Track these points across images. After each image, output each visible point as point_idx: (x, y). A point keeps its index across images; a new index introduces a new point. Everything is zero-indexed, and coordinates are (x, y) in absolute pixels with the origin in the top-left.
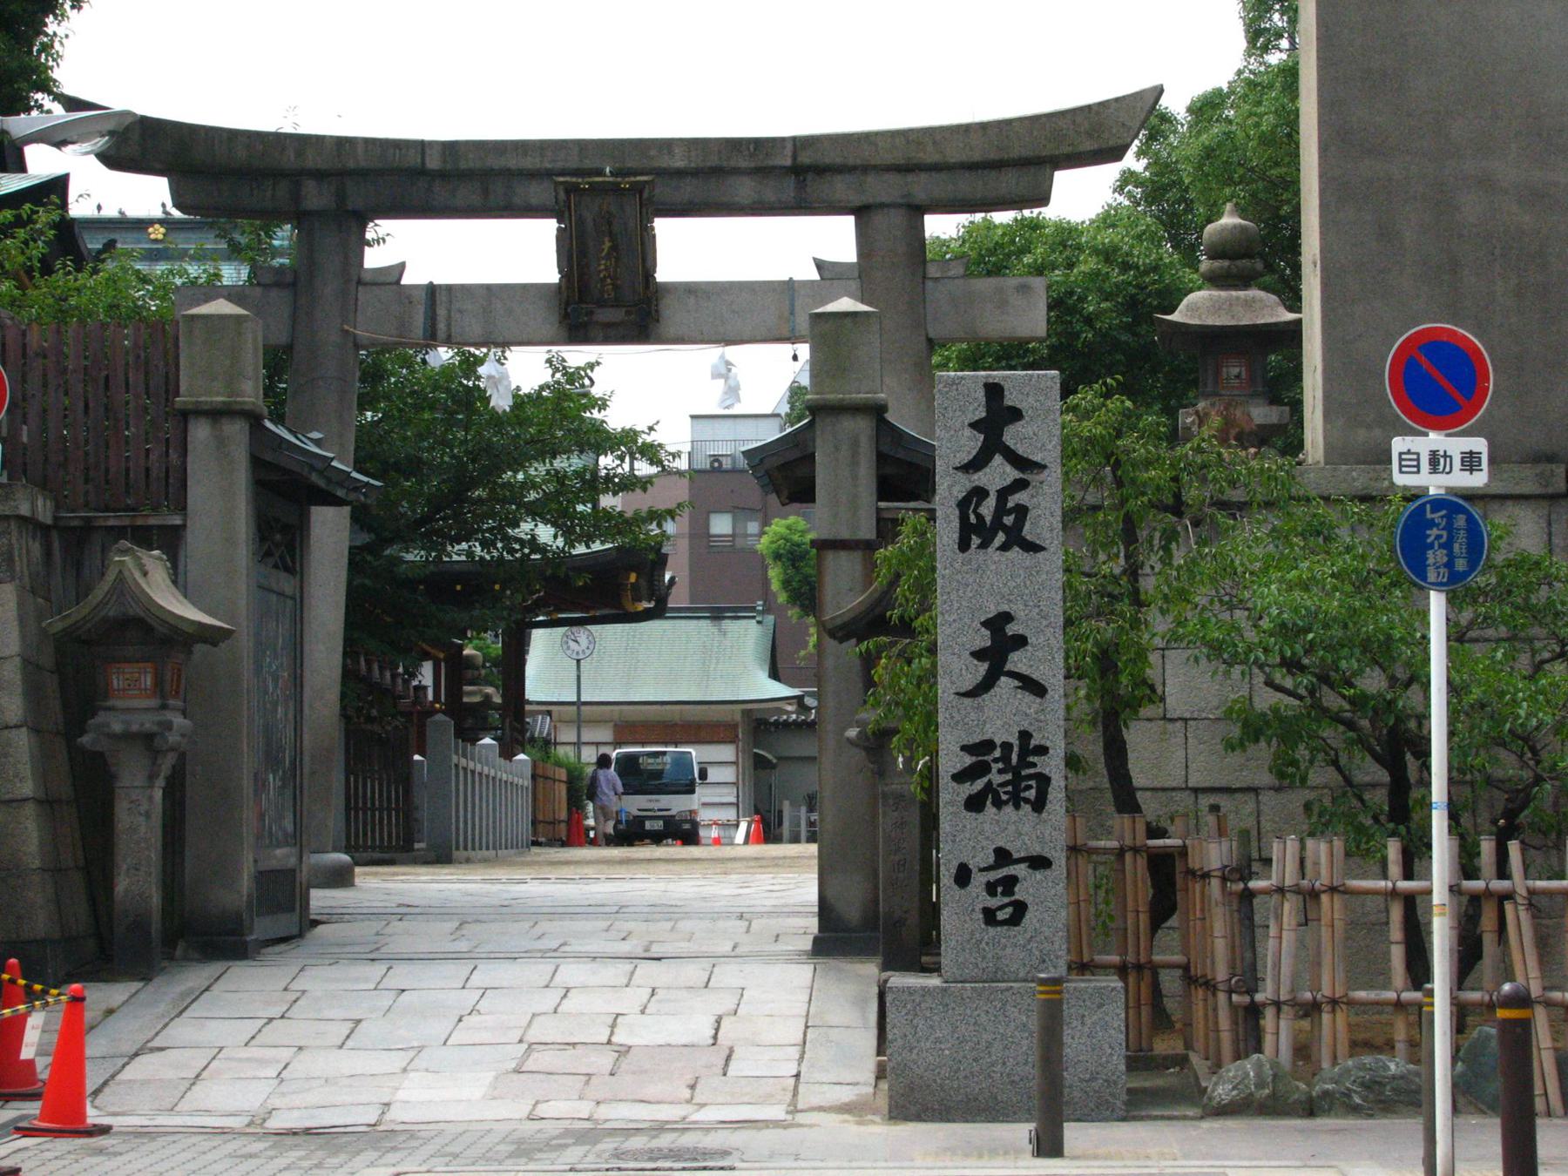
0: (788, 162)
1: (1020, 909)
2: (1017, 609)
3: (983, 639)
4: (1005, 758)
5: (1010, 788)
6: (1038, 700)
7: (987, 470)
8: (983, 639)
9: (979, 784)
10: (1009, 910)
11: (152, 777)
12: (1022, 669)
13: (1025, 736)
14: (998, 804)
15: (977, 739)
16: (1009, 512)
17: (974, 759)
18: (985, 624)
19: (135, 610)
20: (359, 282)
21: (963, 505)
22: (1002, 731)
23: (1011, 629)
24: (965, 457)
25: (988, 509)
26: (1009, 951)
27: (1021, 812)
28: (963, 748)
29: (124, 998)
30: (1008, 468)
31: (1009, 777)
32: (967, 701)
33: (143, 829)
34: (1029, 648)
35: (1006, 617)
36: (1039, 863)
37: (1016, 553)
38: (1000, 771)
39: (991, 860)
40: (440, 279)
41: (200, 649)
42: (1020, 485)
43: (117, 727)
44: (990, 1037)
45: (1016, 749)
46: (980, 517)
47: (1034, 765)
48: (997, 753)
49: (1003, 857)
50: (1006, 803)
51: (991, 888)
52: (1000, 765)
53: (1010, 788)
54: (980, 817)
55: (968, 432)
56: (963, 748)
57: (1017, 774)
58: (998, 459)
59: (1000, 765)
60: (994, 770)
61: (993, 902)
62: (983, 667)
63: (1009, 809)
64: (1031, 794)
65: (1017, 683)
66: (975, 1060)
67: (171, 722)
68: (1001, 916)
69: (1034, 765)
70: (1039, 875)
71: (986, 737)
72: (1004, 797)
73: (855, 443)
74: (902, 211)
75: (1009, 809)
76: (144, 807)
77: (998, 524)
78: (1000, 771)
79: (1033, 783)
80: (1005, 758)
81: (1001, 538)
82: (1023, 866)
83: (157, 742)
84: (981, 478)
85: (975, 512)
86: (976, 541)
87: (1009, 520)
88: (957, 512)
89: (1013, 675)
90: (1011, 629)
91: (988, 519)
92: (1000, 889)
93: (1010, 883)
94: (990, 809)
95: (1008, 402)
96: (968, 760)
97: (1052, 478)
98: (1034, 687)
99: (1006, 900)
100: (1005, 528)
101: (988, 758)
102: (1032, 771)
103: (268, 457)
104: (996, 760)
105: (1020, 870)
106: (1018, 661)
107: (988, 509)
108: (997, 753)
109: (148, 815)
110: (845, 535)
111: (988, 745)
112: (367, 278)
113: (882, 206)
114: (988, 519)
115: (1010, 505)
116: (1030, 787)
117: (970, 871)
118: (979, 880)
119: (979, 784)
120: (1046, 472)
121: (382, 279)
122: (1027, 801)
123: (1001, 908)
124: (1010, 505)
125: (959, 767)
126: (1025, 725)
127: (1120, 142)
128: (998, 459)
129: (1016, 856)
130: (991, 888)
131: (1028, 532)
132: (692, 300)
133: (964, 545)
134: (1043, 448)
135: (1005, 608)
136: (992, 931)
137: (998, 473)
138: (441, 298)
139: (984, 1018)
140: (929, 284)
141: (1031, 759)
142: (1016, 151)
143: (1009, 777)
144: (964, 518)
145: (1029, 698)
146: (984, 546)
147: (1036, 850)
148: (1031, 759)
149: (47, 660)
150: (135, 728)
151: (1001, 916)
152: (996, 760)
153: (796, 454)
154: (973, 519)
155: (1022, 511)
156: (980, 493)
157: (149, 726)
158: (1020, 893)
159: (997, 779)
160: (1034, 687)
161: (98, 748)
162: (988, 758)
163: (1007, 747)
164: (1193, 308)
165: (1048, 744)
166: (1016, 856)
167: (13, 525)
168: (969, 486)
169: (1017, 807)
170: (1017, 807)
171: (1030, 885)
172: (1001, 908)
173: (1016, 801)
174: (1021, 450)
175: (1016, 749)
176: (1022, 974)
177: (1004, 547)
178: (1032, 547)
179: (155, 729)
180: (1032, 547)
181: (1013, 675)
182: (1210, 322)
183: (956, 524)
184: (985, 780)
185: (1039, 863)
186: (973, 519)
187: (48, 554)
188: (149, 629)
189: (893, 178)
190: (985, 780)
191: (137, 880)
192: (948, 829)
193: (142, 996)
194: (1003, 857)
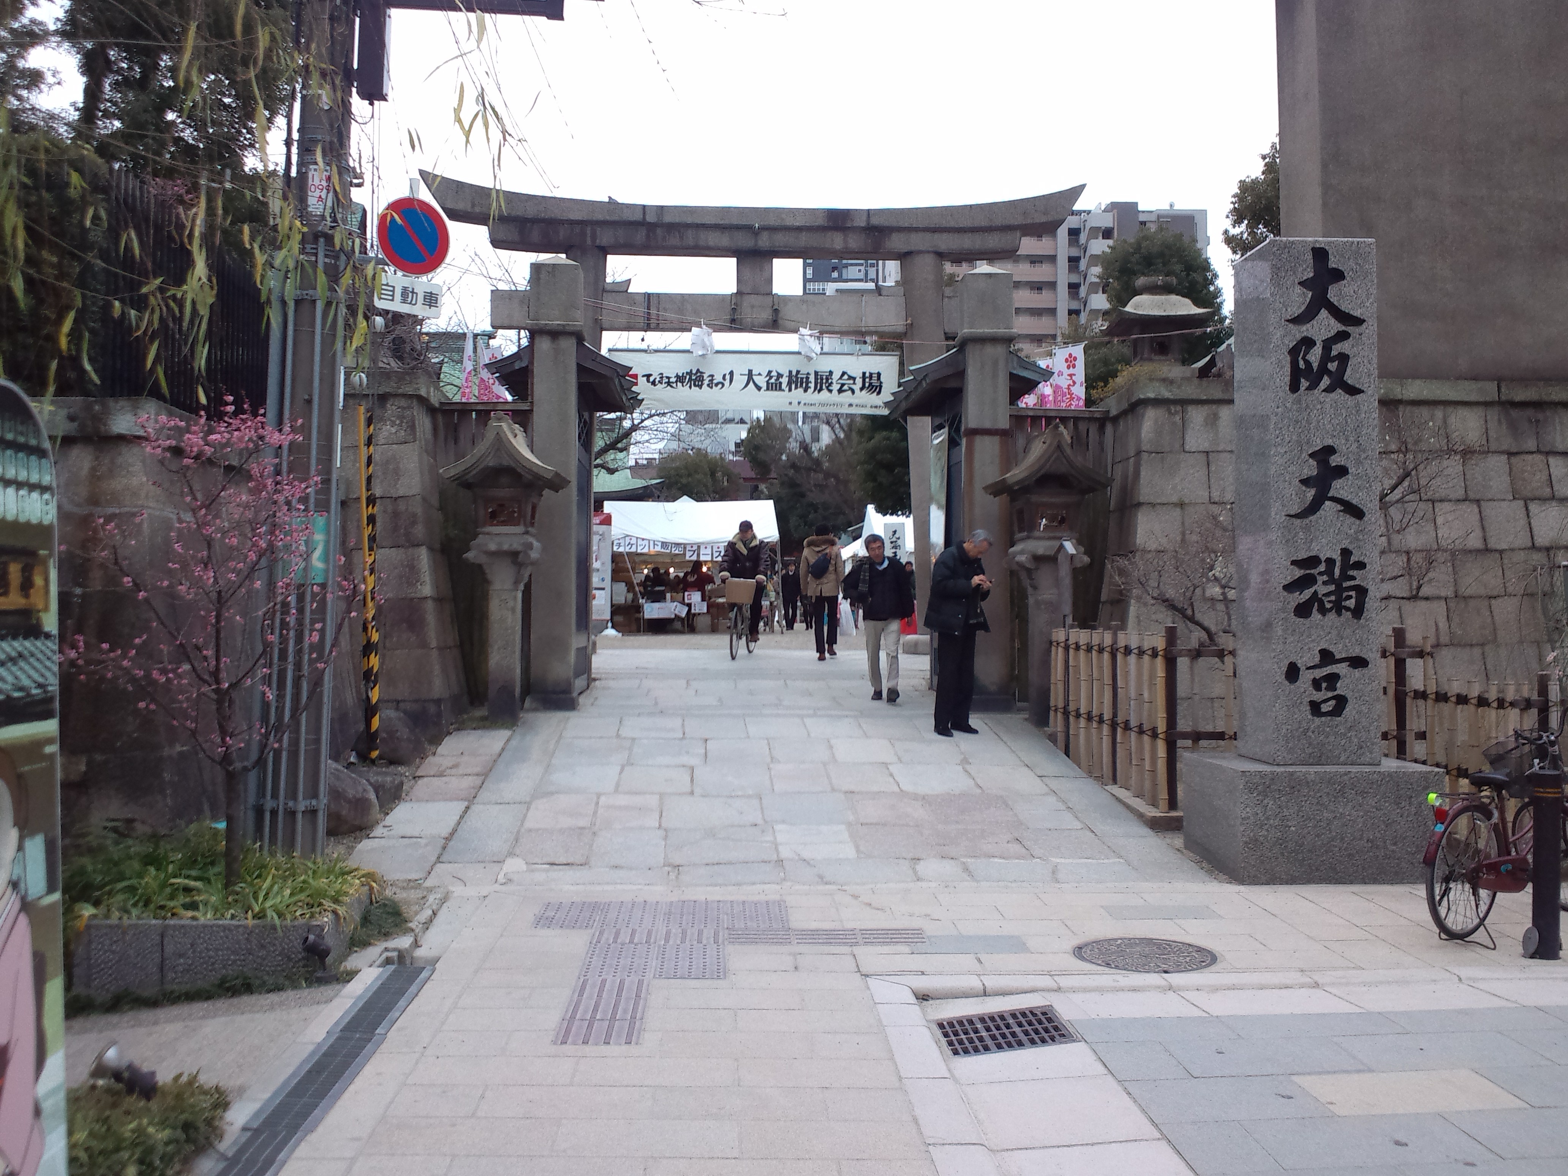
0: (863, 224)
1: (1341, 702)
2: (1338, 443)
3: (1311, 469)
4: (1329, 571)
5: (1333, 598)
6: (1358, 522)
7: (1314, 322)
8: (1311, 469)
9: (1307, 594)
10: (1332, 703)
11: (516, 582)
12: (1343, 494)
13: (1346, 553)
14: (1323, 611)
15: (1302, 555)
16: (1332, 360)
17: (1302, 572)
18: (1312, 455)
19: (506, 462)
20: (604, 290)
21: (1294, 352)
22: (1327, 548)
23: (1335, 460)
24: (1297, 309)
25: (1315, 356)
26: (1332, 738)
27: (1342, 618)
28: (1294, 563)
29: (501, 744)
30: (1332, 321)
31: (1332, 588)
32: (1297, 522)
33: (510, 620)
34: (1350, 477)
35: (1330, 450)
36: (1358, 662)
37: (1339, 394)
38: (1325, 583)
39: (1317, 660)
40: (650, 290)
41: (546, 492)
42: (1342, 336)
43: (493, 547)
44: (1331, 816)
45: (1338, 564)
46: (1308, 363)
47: (1353, 578)
48: (1322, 568)
49: (1327, 657)
50: (1331, 610)
51: (1316, 684)
52: (1325, 578)
53: (1333, 598)
54: (1307, 622)
55: (1298, 289)
56: (1294, 563)
57: (1339, 587)
58: (1324, 313)
59: (1325, 578)
60: (1320, 582)
61: (1318, 696)
62: (1311, 493)
63: (1332, 616)
64: (1351, 603)
65: (1339, 507)
66: (1318, 836)
67: (531, 544)
68: (1325, 708)
69: (1353, 578)
70: (1357, 673)
71: (1312, 554)
72: (1328, 606)
73: (995, 363)
74: (932, 255)
75: (1332, 616)
76: (511, 604)
77: (1323, 370)
78: (1325, 583)
79: (1353, 593)
80: (1329, 571)
81: (1326, 381)
82: (1344, 665)
83: (521, 558)
84: (1306, 330)
85: (1304, 358)
86: (1304, 383)
87: (1332, 366)
88: (1289, 358)
89: (1334, 499)
90: (1335, 460)
91: (1315, 365)
92: (1324, 685)
93: (1332, 679)
94: (1316, 615)
95: (1332, 264)
96: (1298, 573)
97: (1370, 329)
98: (1355, 511)
99: (1330, 694)
100: (1329, 373)
101: (1314, 572)
102: (1352, 583)
103: (589, 364)
104: (1321, 574)
105: (1342, 669)
106: (1340, 488)
107: (1315, 356)
108: (1322, 568)
109: (513, 610)
110: (987, 425)
111: (1313, 561)
112: (608, 288)
113: (920, 252)
114: (1315, 365)
115: (1334, 353)
116: (1350, 597)
117: (1299, 669)
118: (1306, 677)
119: (1307, 594)
120: (1364, 325)
121: (617, 289)
122: (1348, 609)
123: (1326, 701)
124: (1334, 353)
125: (1289, 579)
126: (1345, 544)
127: (1061, 217)
128: (1324, 313)
129: (1338, 657)
130: (1316, 684)
131: (1349, 377)
132: (804, 307)
133: (1294, 387)
134: (1362, 305)
135: (1330, 442)
136: (1317, 721)
137: (1324, 326)
138: (653, 302)
139: (1325, 799)
140: (946, 300)
141: (1351, 573)
142: (998, 222)
143: (1332, 588)
144: (1294, 364)
145: (1350, 520)
146: (1312, 387)
147: (1355, 651)
148: (1351, 573)
149: (435, 501)
150: (506, 547)
151: (1325, 708)
152: (1321, 574)
153: (949, 371)
154: (1302, 364)
155: (1344, 359)
156: (1308, 343)
157: (516, 546)
158: (1341, 688)
159: (1321, 589)
160: (1355, 511)
161: (478, 561)
162: (1314, 572)
163: (1330, 562)
164: (1136, 307)
165: (1366, 561)
166: (1338, 657)
167: (415, 402)
168: (1299, 337)
169: (1339, 614)
170: (1339, 614)
171: (1349, 681)
172: (1326, 701)
173: (1339, 608)
174: (1345, 307)
175: (1338, 564)
176: (1342, 759)
177: (1329, 390)
178: (1353, 391)
179: (520, 548)
180: (1353, 391)
181: (1334, 499)
182: (1151, 313)
183: (1288, 369)
184: (1312, 590)
185: (1358, 662)
186: (1302, 364)
187: (435, 429)
188: (520, 476)
189: (928, 236)
190: (1312, 590)
191: (503, 657)
192: (1280, 633)
193: (514, 743)
194: (1327, 657)
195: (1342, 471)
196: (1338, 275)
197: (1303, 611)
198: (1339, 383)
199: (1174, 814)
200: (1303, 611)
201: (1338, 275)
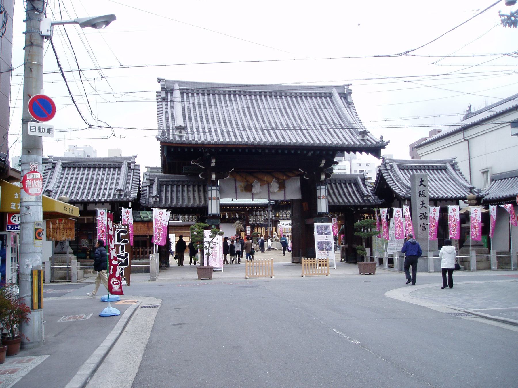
8: (421, 203)
25: (421, 193)
107: (421, 193)
197: (421, 219)
198: (424, 196)
200: (421, 219)
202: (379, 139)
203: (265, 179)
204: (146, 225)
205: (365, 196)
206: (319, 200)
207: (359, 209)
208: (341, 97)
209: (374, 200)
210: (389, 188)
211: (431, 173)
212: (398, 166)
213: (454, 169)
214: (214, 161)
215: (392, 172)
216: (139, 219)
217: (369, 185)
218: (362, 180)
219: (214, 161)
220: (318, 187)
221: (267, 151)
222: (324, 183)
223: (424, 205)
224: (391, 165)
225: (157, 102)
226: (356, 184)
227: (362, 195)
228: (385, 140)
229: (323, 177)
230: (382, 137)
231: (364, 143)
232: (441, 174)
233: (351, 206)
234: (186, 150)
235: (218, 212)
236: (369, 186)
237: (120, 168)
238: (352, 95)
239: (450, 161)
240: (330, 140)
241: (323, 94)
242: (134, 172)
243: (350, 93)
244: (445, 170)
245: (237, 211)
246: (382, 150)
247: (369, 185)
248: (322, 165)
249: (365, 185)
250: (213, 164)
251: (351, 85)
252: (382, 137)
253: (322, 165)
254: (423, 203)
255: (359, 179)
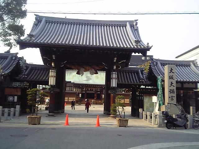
36: (174, 97)
185: (174, 97)
194: (172, 96)
195: (173, 83)
196: (173, 70)
197: (170, 93)
199: (175, 91)
200: (170, 93)
201: (173, 70)
202: (146, 44)
203: (87, 68)
204: (16, 90)
205: (141, 79)
206: (112, 80)
207: (137, 87)
208: (131, 27)
209: (146, 82)
210: (154, 75)
211: (186, 69)
212: (161, 63)
213: (195, 66)
214: (54, 56)
215: (157, 67)
216: (11, 86)
217: (145, 74)
218: (141, 71)
219: (54, 56)
220: (112, 73)
221: (87, 50)
222: (114, 71)
223: (172, 85)
224: (156, 63)
225: (33, 26)
226: (138, 73)
227: (139, 78)
228: (150, 45)
229: (115, 67)
230: (148, 44)
231: (136, 47)
232: (187, 68)
233: (133, 85)
234: (87, 50)
235: (54, 84)
236: (145, 75)
237: (7, 59)
238: (138, 26)
239: (193, 62)
240: (126, 45)
241: (122, 25)
242: (14, 61)
243: (136, 24)
244: (189, 66)
245: (89, 87)
246: (148, 52)
247: (145, 74)
248: (115, 61)
249: (142, 74)
250: (54, 58)
251: (137, 20)
252: (148, 44)
253: (115, 61)
254: (172, 83)
255: (139, 70)
